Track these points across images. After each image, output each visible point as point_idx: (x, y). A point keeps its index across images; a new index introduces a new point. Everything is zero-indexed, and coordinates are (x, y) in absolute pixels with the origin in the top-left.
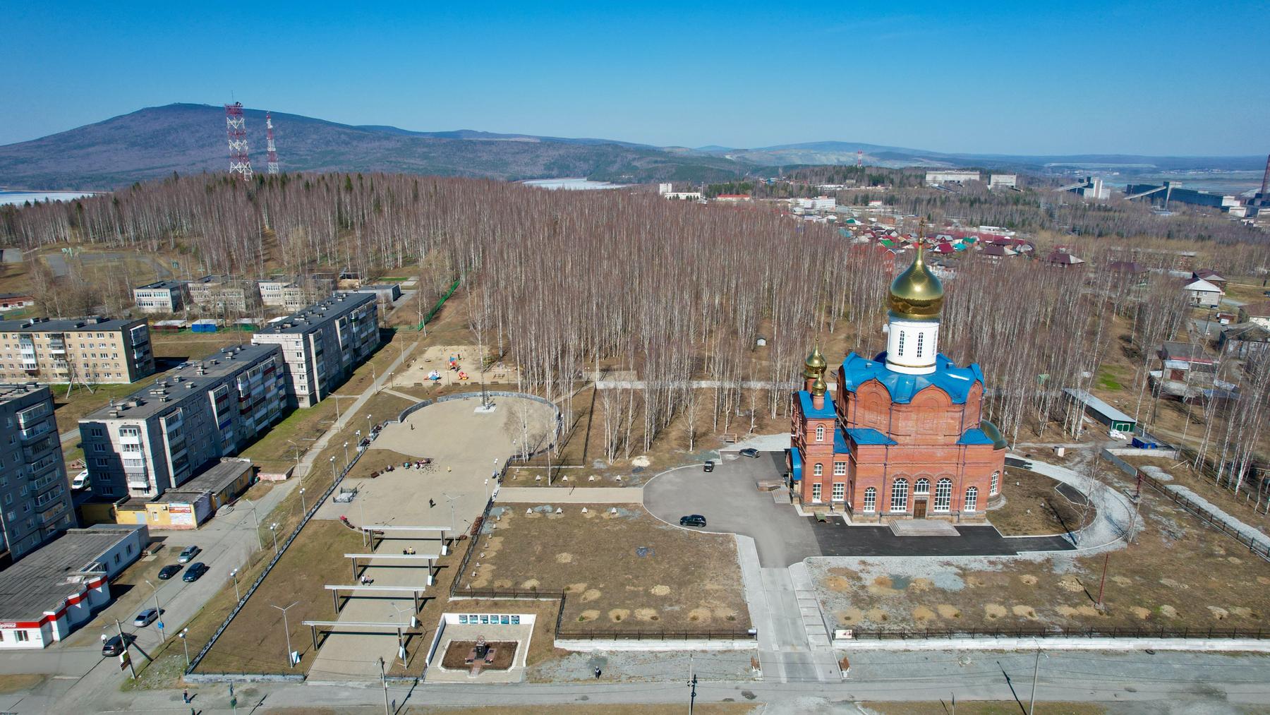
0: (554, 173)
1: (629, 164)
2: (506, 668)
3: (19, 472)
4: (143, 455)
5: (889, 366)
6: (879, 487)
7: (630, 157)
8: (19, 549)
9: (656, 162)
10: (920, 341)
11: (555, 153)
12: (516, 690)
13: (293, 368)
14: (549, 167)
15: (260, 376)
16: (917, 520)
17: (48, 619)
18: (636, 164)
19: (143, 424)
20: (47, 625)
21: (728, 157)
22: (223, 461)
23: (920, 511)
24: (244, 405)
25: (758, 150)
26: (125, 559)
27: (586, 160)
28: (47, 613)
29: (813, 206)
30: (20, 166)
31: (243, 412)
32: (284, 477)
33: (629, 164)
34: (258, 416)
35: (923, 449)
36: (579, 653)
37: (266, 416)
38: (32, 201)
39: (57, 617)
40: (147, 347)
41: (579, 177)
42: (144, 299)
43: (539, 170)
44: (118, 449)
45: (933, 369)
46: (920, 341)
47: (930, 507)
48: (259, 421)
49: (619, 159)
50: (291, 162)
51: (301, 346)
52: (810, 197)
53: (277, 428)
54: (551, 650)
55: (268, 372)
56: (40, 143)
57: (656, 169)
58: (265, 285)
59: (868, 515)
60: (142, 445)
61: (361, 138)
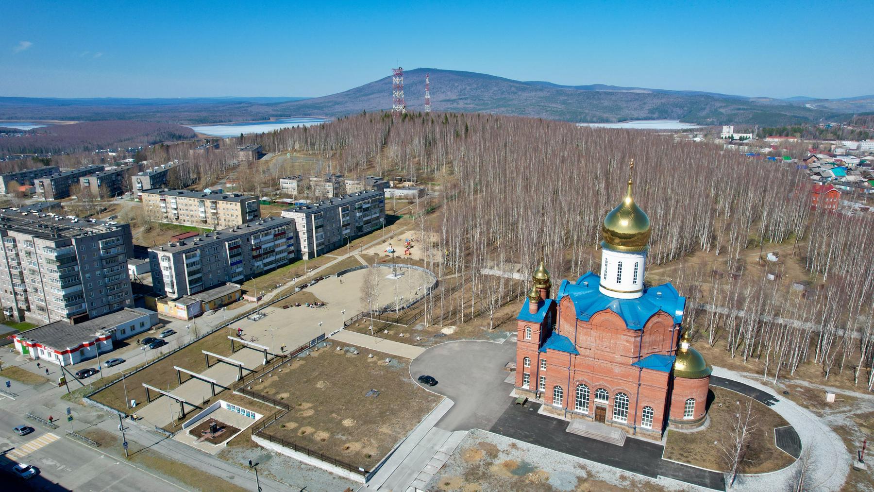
0: (655, 116)
1: (716, 110)
2: (216, 444)
3: (98, 272)
4: (171, 273)
5: (601, 290)
6: (565, 388)
7: (718, 104)
8: (94, 313)
9: (739, 109)
10: (620, 269)
11: (658, 102)
12: (207, 459)
13: (301, 234)
14: (652, 111)
15: (271, 237)
16: (597, 423)
17: (67, 352)
18: (723, 111)
19: (171, 255)
20: (67, 355)
21: (808, 106)
22: (228, 284)
23: (600, 415)
24: (255, 253)
25: (839, 100)
26: (138, 329)
27: (682, 107)
28: (68, 349)
29: (858, 148)
30: (337, 106)
31: (254, 257)
32: (255, 299)
33: (716, 110)
34: (266, 261)
35: (602, 363)
36: (262, 448)
37: (275, 261)
38: (301, 125)
39: (72, 351)
40: (256, 213)
41: (674, 119)
42: (285, 185)
43: (643, 114)
44: (162, 269)
45: (638, 295)
46: (620, 269)
47: (608, 414)
48: (265, 265)
49: (708, 107)
50: (478, 105)
51: (305, 221)
52: (858, 141)
53: (279, 270)
54: (249, 440)
55: (282, 234)
56: (348, 94)
57: (735, 115)
58: (349, 182)
59: (557, 408)
60: (170, 268)
61: (524, 90)
